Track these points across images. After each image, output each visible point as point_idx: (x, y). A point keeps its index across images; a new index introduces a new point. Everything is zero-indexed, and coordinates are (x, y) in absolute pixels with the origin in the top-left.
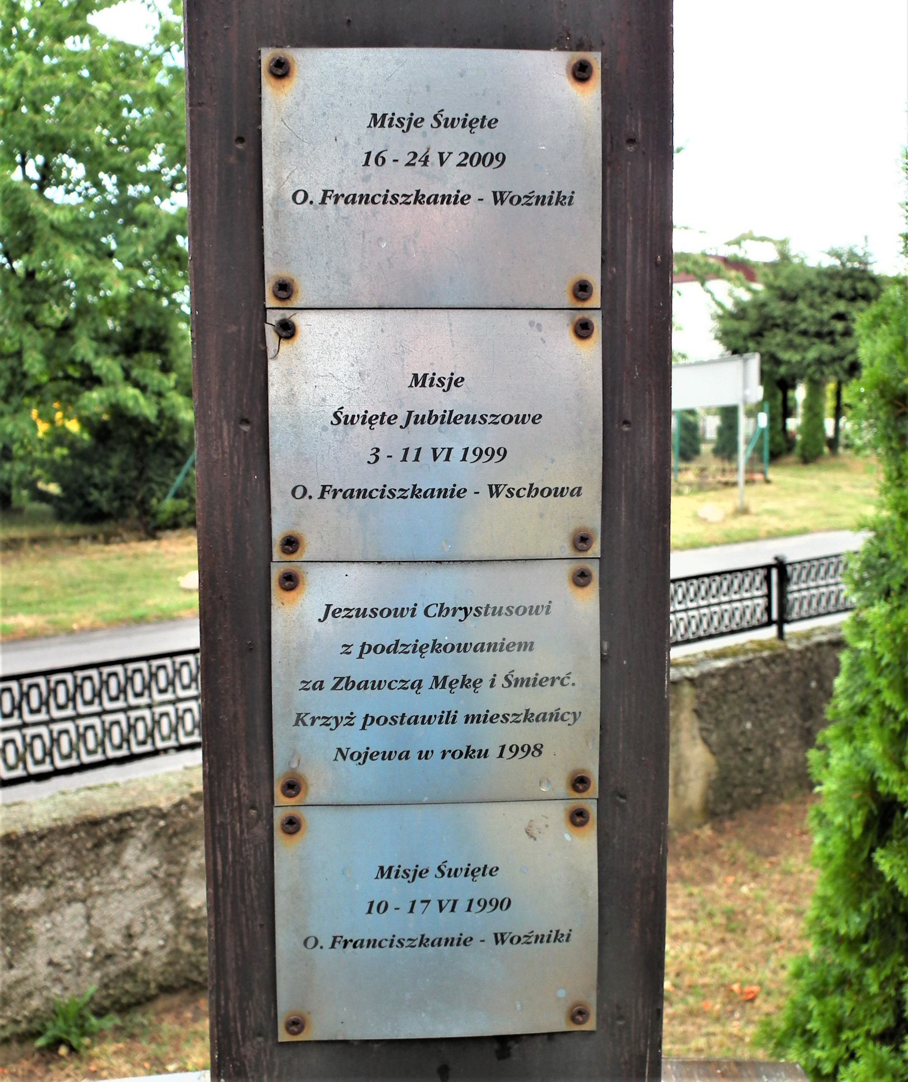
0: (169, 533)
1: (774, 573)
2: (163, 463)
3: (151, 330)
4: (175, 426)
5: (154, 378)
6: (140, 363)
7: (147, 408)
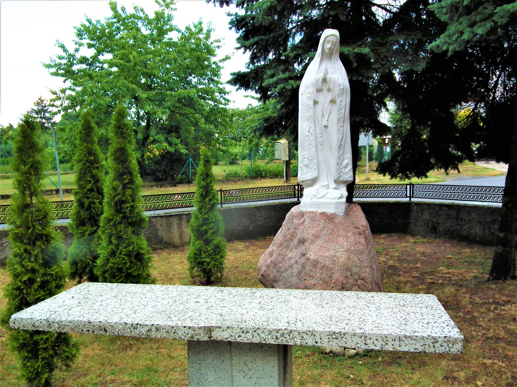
0: (180, 185)
1: (408, 186)
2: (178, 165)
3: (175, 126)
4: (181, 154)
5: (174, 140)
6: (171, 136)
7: (171, 150)
